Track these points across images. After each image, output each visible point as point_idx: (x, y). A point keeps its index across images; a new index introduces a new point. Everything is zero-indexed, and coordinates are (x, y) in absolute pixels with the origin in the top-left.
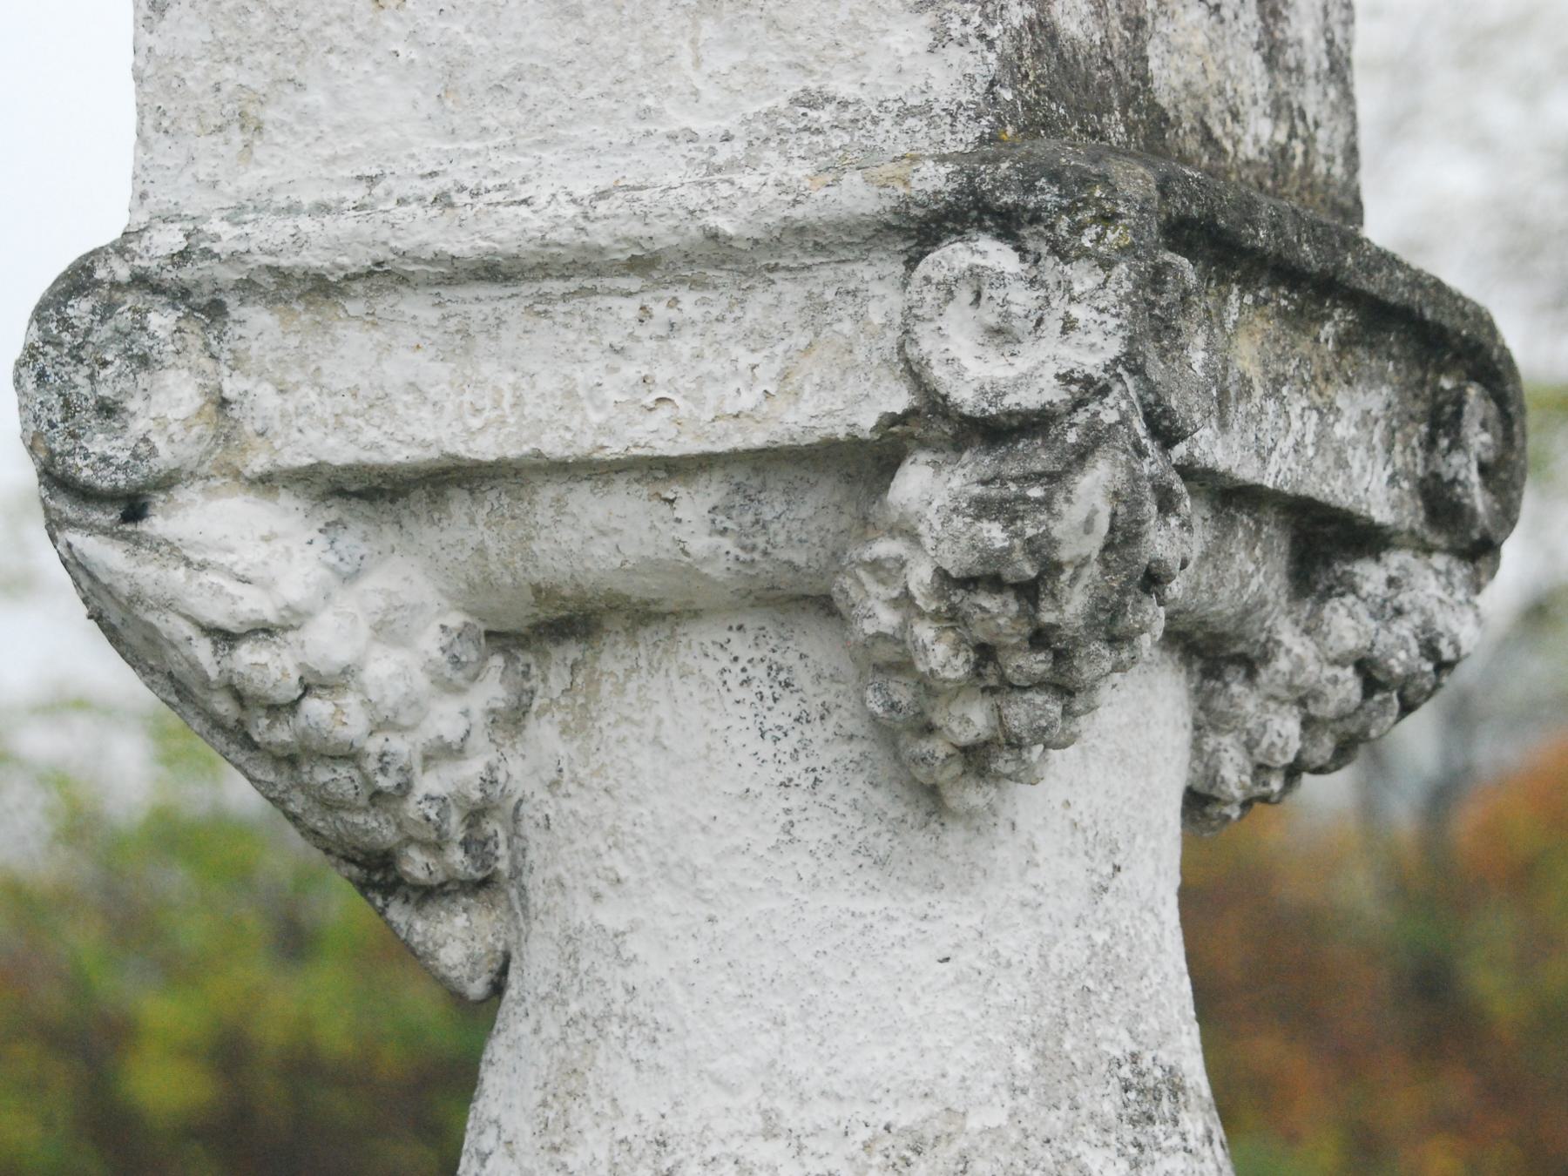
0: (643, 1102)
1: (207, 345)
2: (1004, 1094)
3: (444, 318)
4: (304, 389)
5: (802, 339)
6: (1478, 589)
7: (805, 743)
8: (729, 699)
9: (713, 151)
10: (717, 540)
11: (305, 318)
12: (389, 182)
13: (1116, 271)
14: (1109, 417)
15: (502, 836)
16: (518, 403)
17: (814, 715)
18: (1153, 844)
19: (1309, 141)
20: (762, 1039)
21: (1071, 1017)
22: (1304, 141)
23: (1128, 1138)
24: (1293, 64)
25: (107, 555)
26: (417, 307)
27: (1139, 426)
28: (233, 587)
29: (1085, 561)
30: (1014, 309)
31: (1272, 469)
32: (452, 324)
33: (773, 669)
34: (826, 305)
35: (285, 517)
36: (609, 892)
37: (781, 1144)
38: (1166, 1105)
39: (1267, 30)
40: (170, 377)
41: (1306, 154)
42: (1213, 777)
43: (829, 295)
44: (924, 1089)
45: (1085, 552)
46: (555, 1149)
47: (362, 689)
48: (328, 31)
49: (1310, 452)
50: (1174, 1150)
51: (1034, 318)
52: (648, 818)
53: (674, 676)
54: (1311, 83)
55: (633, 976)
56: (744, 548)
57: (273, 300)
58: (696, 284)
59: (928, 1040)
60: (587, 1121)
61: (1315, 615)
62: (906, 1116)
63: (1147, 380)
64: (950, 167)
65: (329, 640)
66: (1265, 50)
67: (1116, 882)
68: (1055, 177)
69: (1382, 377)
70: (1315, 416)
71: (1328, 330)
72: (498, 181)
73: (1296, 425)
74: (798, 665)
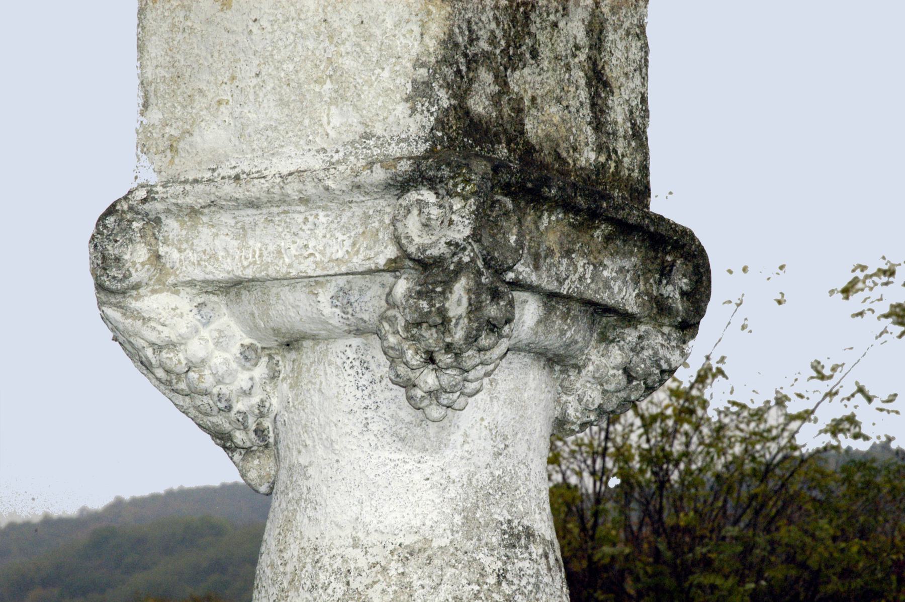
0: (310, 532)
1: (154, 234)
2: (449, 532)
3: (236, 223)
4: (188, 251)
5: (360, 230)
6: (684, 342)
7: (373, 391)
8: (346, 374)
9: (332, 157)
10: (334, 309)
11: (188, 223)
12: (220, 170)
13: (469, 201)
14: (466, 259)
15: (271, 429)
16: (261, 256)
17: (377, 381)
18: (527, 437)
19: (619, 163)
20: (354, 508)
21: (481, 504)
22: (616, 162)
23: (502, 553)
24: (611, 131)
25: (114, 314)
26: (226, 218)
27: (480, 263)
28: (160, 328)
29: (460, 317)
30: (432, 216)
31: (566, 286)
32: (239, 225)
33: (362, 362)
34: (369, 217)
35: (184, 302)
36: (303, 450)
37: (359, 550)
38: (523, 541)
39: (595, 117)
40: (138, 247)
41: (616, 167)
42: (564, 413)
43: (371, 212)
44: (415, 530)
45: (459, 313)
46: (281, 551)
47: (210, 368)
48: (202, 113)
49: (589, 281)
50: (524, 559)
51: (440, 220)
52: (316, 420)
53: (326, 365)
54: (621, 140)
55: (310, 483)
56: (344, 313)
57: (177, 217)
58: (324, 208)
59: (418, 510)
60: (292, 540)
61: (606, 349)
62: (409, 540)
63: (482, 245)
64: (412, 161)
65: (196, 349)
66: (595, 125)
67: (506, 451)
68: (448, 165)
69: (631, 253)
70: (591, 267)
71: (598, 232)
72: (257, 169)
73: (581, 270)
74: (372, 361)
